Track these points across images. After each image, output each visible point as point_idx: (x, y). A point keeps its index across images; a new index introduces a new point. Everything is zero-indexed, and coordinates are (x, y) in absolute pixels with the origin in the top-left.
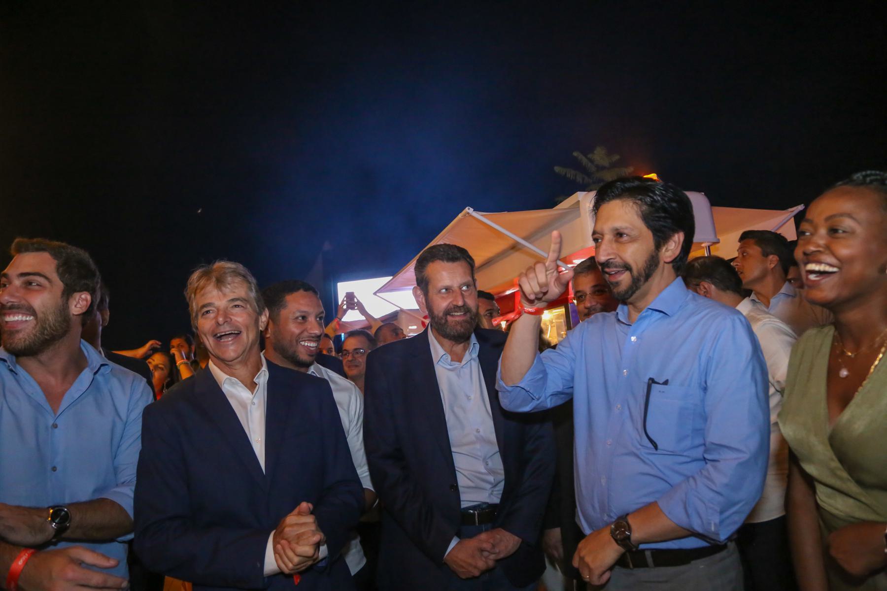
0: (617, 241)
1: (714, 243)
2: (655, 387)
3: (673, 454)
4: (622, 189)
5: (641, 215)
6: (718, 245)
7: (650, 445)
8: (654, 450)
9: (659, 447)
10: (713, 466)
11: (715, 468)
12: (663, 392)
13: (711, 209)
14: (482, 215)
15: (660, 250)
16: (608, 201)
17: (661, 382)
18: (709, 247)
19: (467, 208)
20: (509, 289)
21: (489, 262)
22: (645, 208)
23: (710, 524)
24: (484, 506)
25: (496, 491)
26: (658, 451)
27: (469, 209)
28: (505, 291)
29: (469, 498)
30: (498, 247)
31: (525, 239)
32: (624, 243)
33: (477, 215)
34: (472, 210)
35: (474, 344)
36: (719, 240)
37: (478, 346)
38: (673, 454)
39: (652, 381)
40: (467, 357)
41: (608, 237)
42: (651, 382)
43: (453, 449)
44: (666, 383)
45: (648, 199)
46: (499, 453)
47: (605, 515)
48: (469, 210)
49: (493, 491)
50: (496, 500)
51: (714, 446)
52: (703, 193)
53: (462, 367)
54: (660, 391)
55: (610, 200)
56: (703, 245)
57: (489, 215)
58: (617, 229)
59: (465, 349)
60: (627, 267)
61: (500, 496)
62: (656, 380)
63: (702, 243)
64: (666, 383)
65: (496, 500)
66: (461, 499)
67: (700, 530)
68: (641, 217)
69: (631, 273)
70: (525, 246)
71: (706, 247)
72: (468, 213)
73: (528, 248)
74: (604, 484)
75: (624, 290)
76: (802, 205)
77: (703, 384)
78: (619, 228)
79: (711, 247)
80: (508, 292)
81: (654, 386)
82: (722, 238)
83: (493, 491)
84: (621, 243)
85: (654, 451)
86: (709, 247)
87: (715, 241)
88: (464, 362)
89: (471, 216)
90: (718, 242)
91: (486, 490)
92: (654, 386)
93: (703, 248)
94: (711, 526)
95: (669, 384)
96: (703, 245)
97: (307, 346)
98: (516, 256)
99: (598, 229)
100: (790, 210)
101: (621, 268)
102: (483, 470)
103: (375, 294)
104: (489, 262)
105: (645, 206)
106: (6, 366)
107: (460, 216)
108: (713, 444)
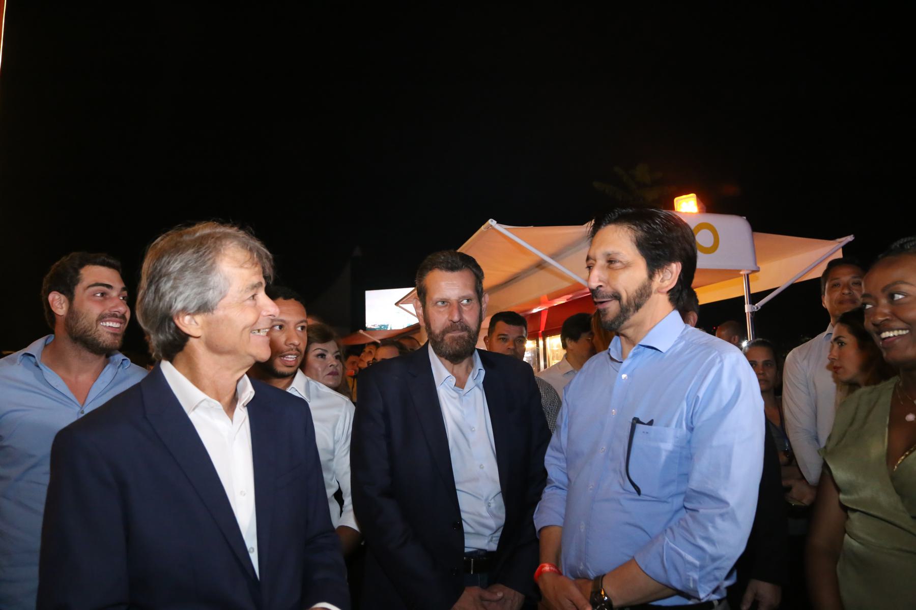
0: (609, 267)
1: (753, 272)
2: (639, 427)
3: (658, 500)
4: (619, 214)
5: (635, 241)
6: (757, 274)
7: (633, 490)
8: (637, 495)
9: (642, 492)
10: (691, 516)
11: (694, 519)
12: (647, 433)
13: (752, 235)
14: (505, 229)
15: (653, 279)
16: (605, 226)
17: (646, 422)
18: (748, 275)
19: (490, 220)
20: (535, 307)
21: (515, 278)
22: (640, 233)
23: (688, 580)
24: (482, 553)
25: (495, 537)
26: (641, 496)
27: (492, 221)
28: (531, 309)
29: (472, 543)
30: (522, 263)
31: (553, 256)
32: (616, 269)
33: (501, 228)
34: (495, 222)
35: (479, 370)
36: (759, 268)
37: (483, 373)
38: (658, 500)
39: (636, 421)
40: (470, 382)
41: (601, 262)
42: (635, 421)
43: (457, 487)
44: (651, 423)
45: (645, 226)
46: (501, 493)
47: (582, 564)
48: (492, 222)
49: (492, 538)
50: (493, 547)
51: (694, 494)
52: (745, 218)
53: (465, 395)
54: (644, 432)
55: (607, 224)
56: (741, 273)
57: (513, 228)
58: (609, 255)
59: (468, 372)
60: (617, 297)
61: (497, 542)
62: (641, 419)
63: (740, 271)
64: (651, 423)
65: (493, 547)
66: (466, 545)
67: (679, 587)
68: (635, 243)
69: (620, 302)
70: (550, 264)
71: (745, 275)
72: (491, 226)
73: (555, 267)
74: (582, 530)
75: (611, 320)
76: (852, 235)
77: (690, 424)
78: (611, 253)
79: (750, 276)
80: (535, 311)
81: (639, 426)
82: (763, 267)
83: (492, 538)
84: (612, 269)
85: (637, 496)
86: (748, 275)
87: (754, 269)
88: (466, 389)
89: (494, 229)
90: (757, 271)
91: (485, 536)
92: (639, 426)
93: (742, 275)
94: (689, 583)
95: (654, 423)
96: (741, 273)
97: (894, 336)
98: (542, 274)
99: (591, 255)
100: (839, 240)
101: (609, 298)
102: (486, 514)
103: (397, 304)
104: (515, 278)
105: (640, 232)
106: (32, 362)
107: (483, 228)
108: (694, 491)
